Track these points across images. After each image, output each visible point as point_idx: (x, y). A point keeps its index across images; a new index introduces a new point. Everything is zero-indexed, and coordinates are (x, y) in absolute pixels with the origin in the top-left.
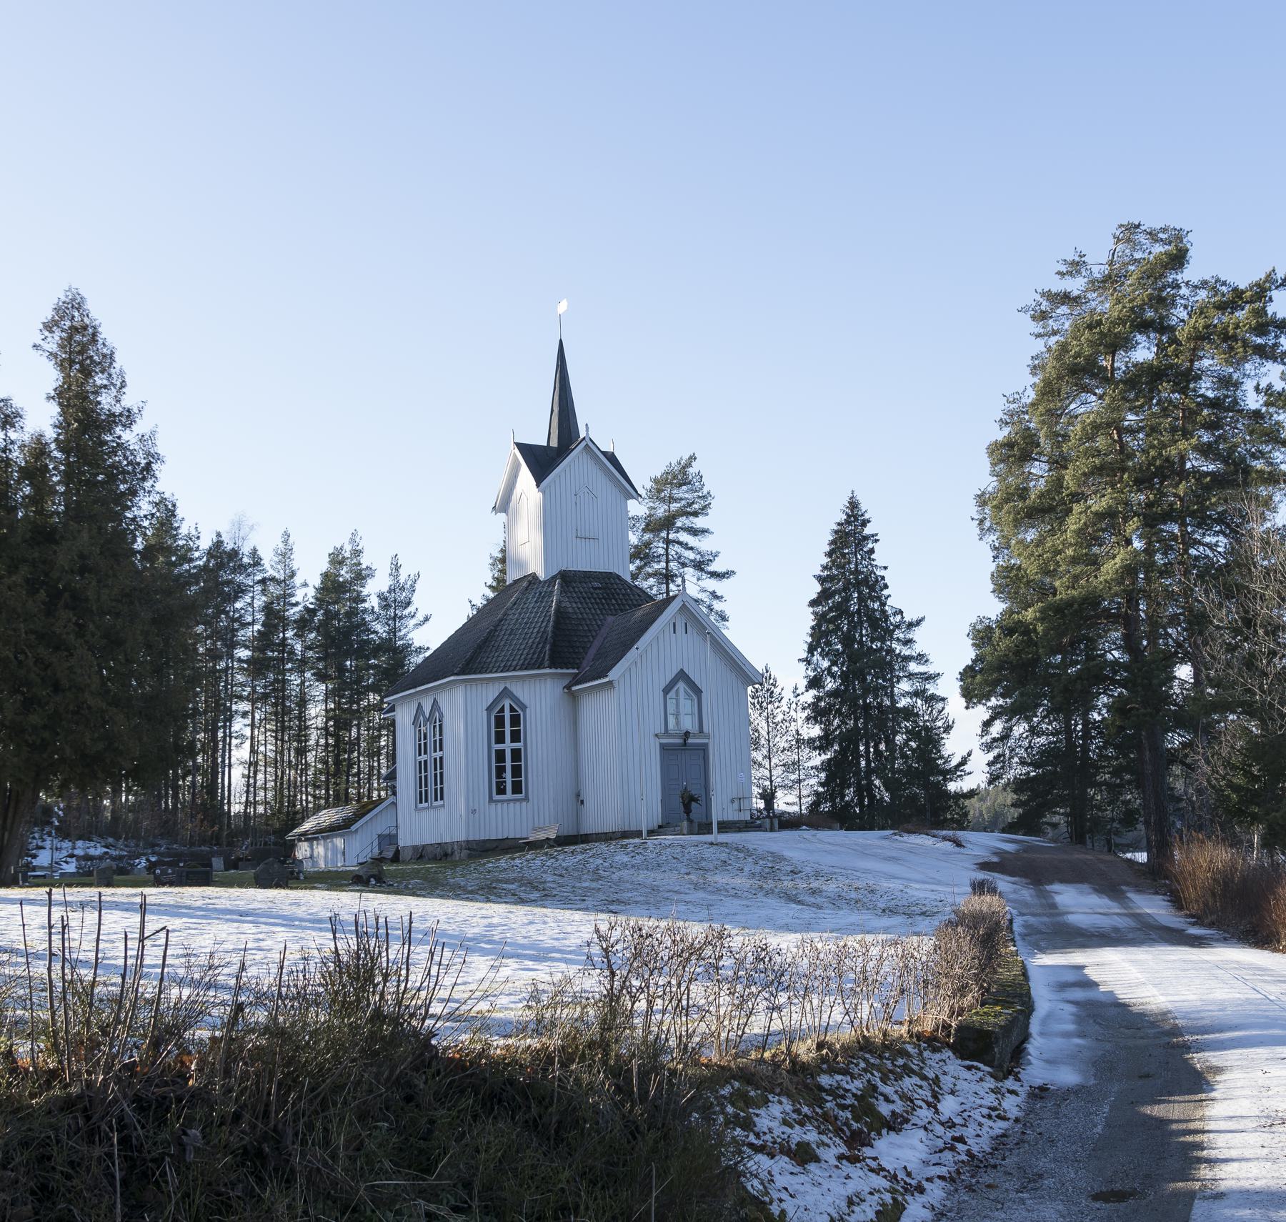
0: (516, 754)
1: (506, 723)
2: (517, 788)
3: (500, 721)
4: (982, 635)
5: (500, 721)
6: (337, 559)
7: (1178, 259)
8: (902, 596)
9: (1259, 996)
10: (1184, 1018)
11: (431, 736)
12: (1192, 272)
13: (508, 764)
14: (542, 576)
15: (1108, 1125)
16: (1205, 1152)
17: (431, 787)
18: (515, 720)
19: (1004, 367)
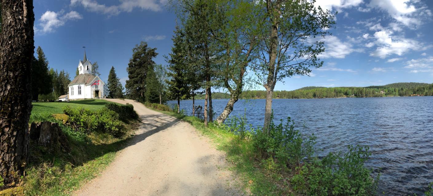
0: (79, 89)
1: (80, 88)
2: (81, 94)
3: (79, 88)
4: (127, 82)
5: (79, 88)
6: (61, 72)
7: (146, 46)
8: (118, 76)
9: (166, 121)
10: (182, 121)
11: (72, 89)
12: (148, 47)
13: (80, 92)
14: (83, 74)
15: (252, 91)
16: (366, 25)
17: (73, 93)
18: (80, 87)
19: (130, 56)
